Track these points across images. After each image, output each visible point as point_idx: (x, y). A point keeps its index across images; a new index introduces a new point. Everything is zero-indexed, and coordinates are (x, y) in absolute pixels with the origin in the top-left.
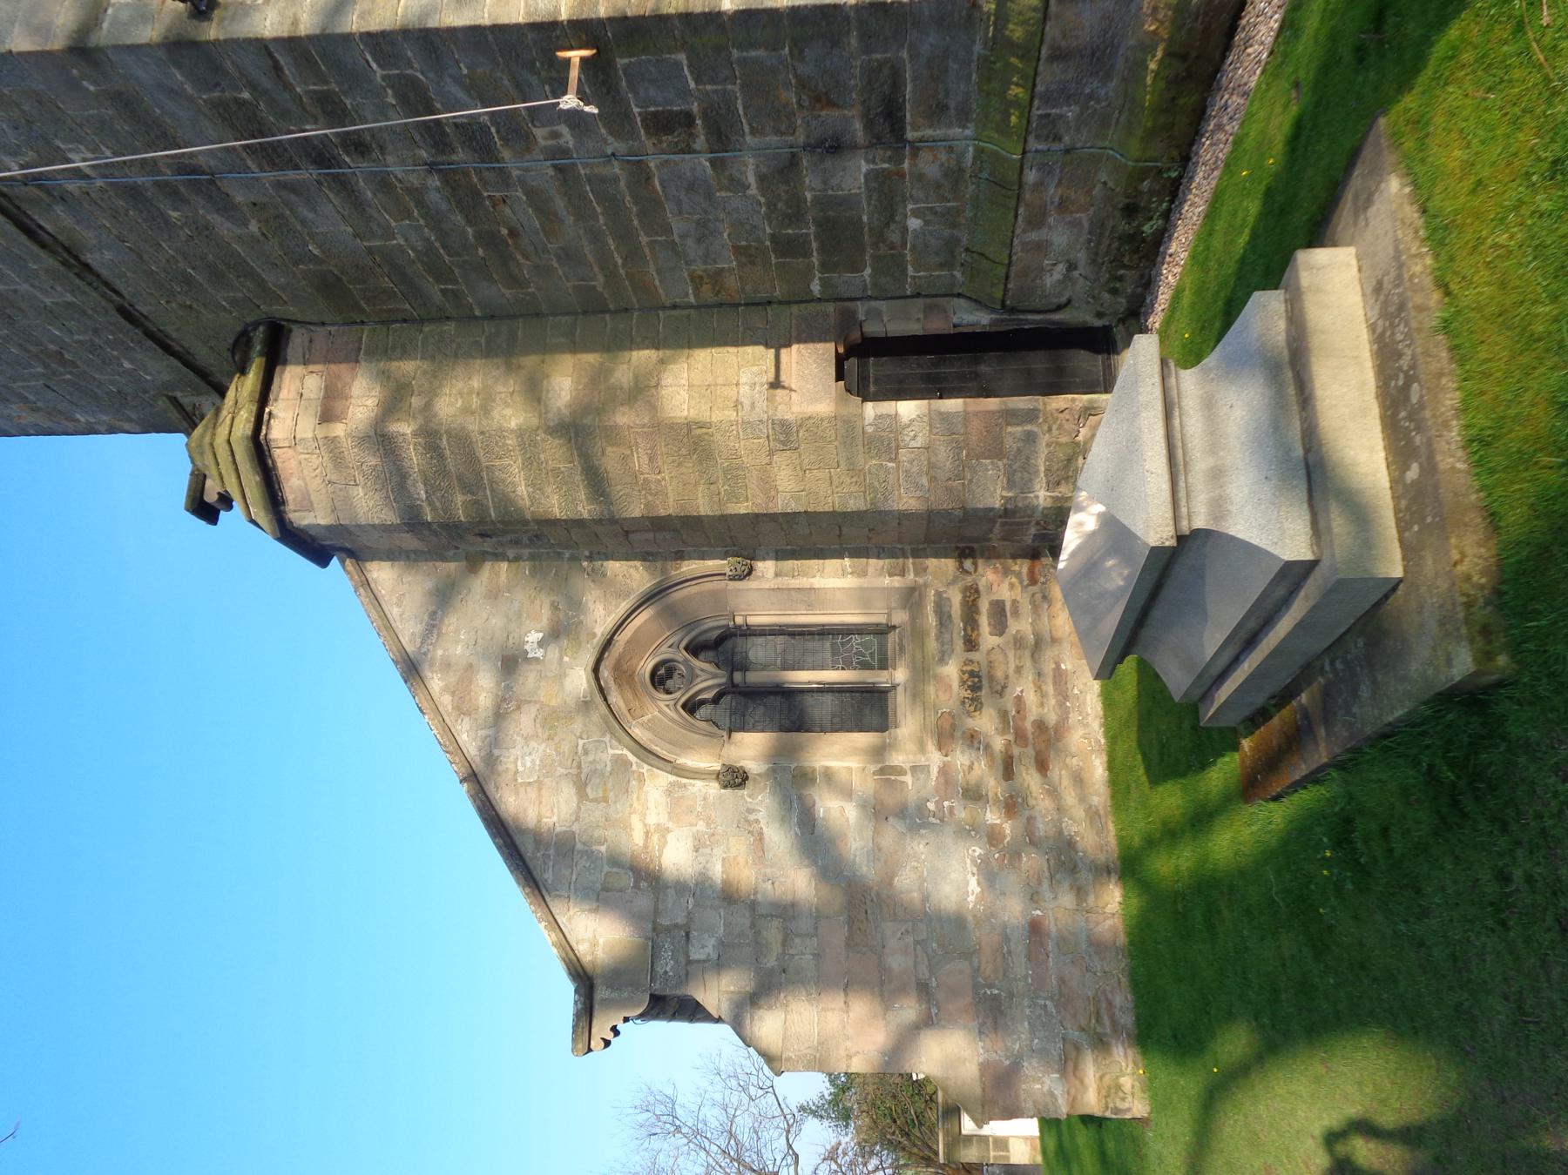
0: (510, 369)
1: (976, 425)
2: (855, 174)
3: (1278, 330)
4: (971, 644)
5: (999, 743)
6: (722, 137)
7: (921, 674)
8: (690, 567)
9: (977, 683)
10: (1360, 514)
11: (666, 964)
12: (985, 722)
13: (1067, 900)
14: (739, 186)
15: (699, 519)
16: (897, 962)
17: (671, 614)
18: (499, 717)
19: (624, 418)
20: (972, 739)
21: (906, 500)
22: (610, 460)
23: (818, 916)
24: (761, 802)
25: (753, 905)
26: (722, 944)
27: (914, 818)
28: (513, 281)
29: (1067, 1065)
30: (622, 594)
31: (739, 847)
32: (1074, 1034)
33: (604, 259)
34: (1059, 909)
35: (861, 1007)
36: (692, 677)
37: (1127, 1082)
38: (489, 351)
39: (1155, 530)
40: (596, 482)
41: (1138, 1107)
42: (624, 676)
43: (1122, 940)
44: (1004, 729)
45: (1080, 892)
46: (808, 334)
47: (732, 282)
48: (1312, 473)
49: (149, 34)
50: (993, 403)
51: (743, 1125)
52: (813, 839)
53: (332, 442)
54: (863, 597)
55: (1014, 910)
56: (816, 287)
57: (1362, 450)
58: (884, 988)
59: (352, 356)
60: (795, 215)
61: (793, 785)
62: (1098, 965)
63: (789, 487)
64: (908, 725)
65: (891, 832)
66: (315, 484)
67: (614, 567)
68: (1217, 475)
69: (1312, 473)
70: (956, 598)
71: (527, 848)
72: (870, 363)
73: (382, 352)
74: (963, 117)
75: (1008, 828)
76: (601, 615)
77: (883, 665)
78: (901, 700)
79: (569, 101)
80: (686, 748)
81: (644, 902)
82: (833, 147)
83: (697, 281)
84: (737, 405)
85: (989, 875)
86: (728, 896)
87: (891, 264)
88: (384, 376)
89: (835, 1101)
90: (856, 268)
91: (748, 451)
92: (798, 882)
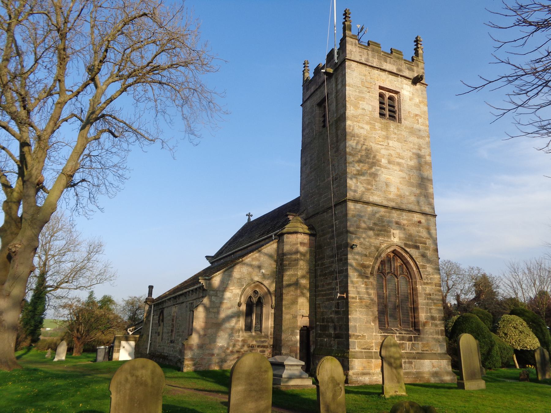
0: (307, 273)
1: (295, 348)
2: (332, 331)
3: (304, 377)
4: (258, 346)
5: (242, 350)
6: (337, 313)
7: (254, 337)
8: (274, 298)
9: (252, 347)
10: (287, 382)
11: (212, 292)
12: (246, 348)
13: (217, 361)
14: (331, 314)
15: (282, 301)
16: (209, 331)
17: (266, 294)
18: (251, 265)
19: (299, 291)
20: (243, 346)
21: (284, 336)
22: (292, 288)
23: (217, 318)
24: (235, 309)
25: (219, 307)
26: (214, 302)
27: (231, 335)
28: (320, 276)
29: (192, 359)
30: (270, 286)
31: (229, 305)
32: (197, 360)
33: (322, 291)
34: (215, 359)
35: (203, 324)
36: (255, 297)
37: (189, 368)
38: (310, 269)
39: (285, 363)
40: (289, 285)
41: (185, 370)
42: (257, 286)
43: (210, 369)
44: (244, 351)
45: (218, 363)
46: (311, 321)
47: (319, 310)
48: (290, 378)
49: (349, 241)
50: (298, 351)
51: (88, 274)
52: (229, 318)
53: (297, 244)
54: (267, 328)
55: (216, 351)
56: (318, 323)
57: (292, 383)
58: (205, 329)
59: (310, 247)
60: (328, 322)
61: (237, 315)
62: (207, 365)
63: (286, 317)
64: (246, 334)
65: (229, 331)
66: (290, 240)
67: (274, 285)
68: (290, 370)
69: (290, 378)
70: (266, 344)
71: (230, 270)
72: (305, 332)
73: (311, 252)
74: (338, 347)
75: (229, 351)
76: (266, 282)
77: (255, 331)
78: (249, 333)
79: (339, 295)
80: (244, 296)
81: (221, 289)
82: (335, 329)
83: (319, 304)
84: (300, 309)
85: (222, 347)
86: (221, 303)
87: (320, 336)
88: (306, 252)
89: (93, 302)
90: (320, 330)
91: (293, 311)
92: (222, 315)
